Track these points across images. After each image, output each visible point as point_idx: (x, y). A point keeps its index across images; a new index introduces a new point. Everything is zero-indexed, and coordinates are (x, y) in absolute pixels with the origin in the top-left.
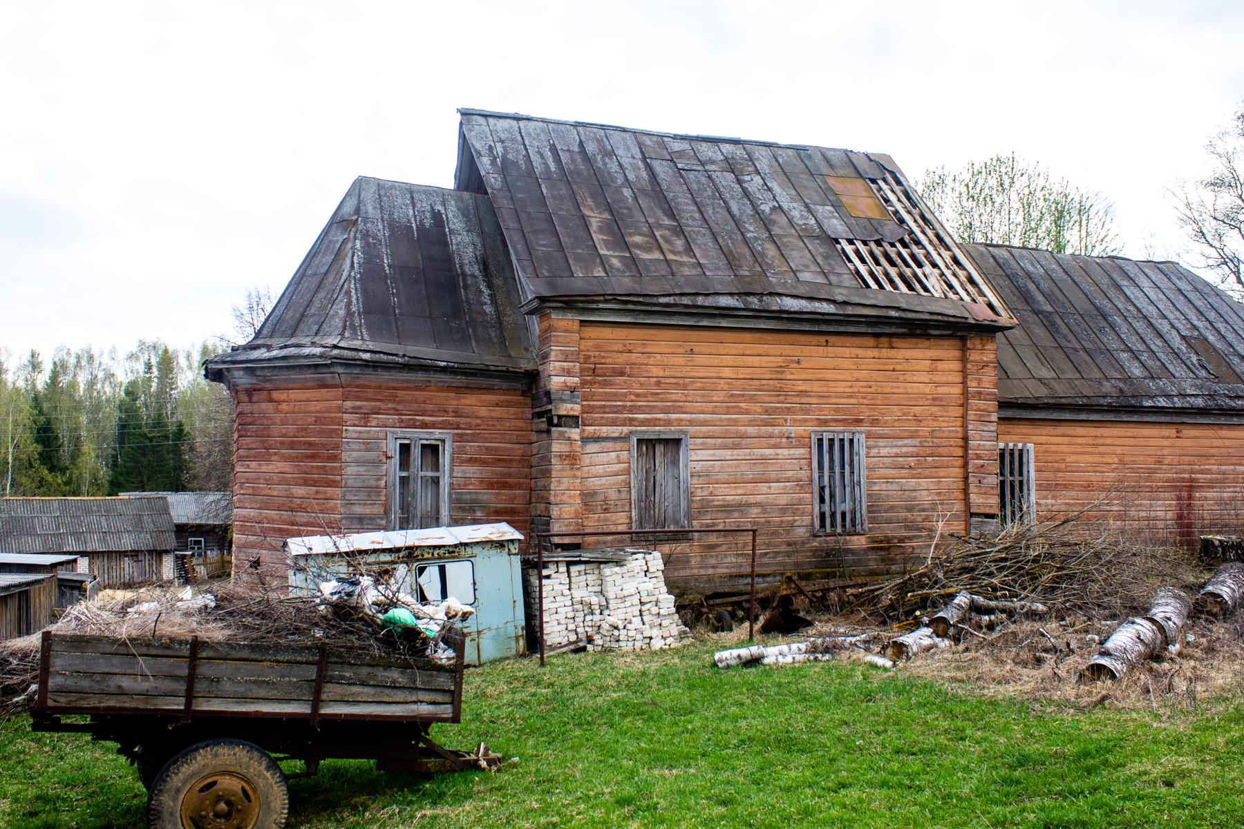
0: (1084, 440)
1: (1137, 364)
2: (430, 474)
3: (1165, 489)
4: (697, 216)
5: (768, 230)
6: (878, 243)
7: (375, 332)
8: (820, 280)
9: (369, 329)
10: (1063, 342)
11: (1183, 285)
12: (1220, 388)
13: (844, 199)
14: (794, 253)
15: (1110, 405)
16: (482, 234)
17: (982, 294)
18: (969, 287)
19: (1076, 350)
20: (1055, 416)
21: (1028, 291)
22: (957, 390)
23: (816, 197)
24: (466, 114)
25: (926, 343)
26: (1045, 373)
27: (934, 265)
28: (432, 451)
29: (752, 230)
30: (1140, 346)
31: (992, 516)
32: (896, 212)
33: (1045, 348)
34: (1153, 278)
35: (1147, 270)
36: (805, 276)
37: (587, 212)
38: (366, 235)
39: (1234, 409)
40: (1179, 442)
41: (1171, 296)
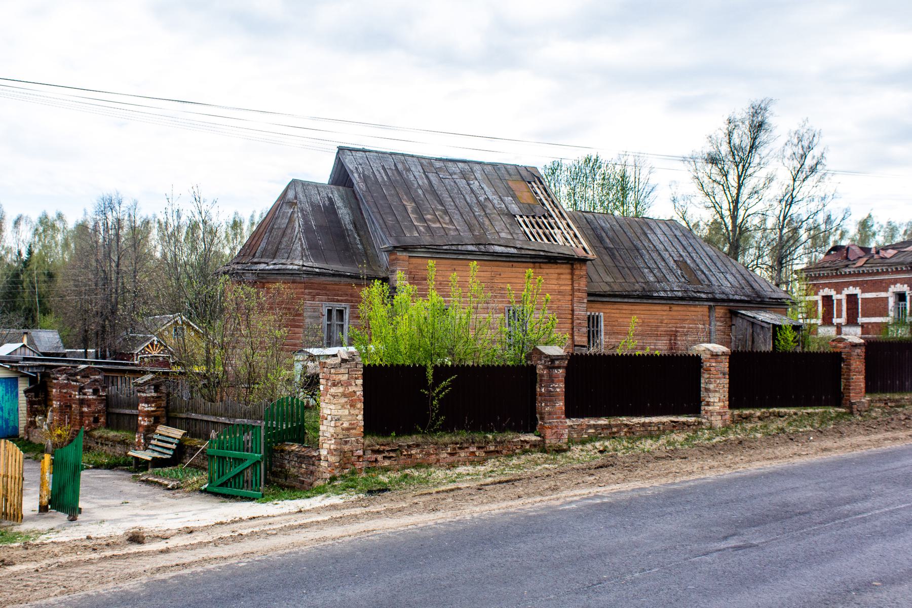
0: (627, 312)
1: (652, 275)
2: (340, 323)
3: (664, 335)
4: (452, 203)
5: (484, 211)
6: (533, 217)
7: (316, 258)
8: (510, 237)
9: (313, 257)
10: (618, 264)
11: (678, 233)
12: (690, 287)
13: (516, 193)
14: (497, 223)
15: (638, 295)
16: (351, 208)
17: (580, 243)
18: (575, 240)
19: (623, 268)
20: (613, 300)
21: (602, 237)
22: (569, 288)
23: (503, 192)
24: (341, 149)
25: (556, 266)
26: (609, 279)
27: (559, 228)
28: (341, 313)
29: (478, 211)
30: (654, 266)
31: (584, 346)
32: (541, 200)
33: (609, 266)
34: (663, 229)
35: (660, 225)
36: (503, 235)
37: (405, 203)
38: (302, 210)
39: (696, 297)
40: (671, 313)
41: (671, 239)
